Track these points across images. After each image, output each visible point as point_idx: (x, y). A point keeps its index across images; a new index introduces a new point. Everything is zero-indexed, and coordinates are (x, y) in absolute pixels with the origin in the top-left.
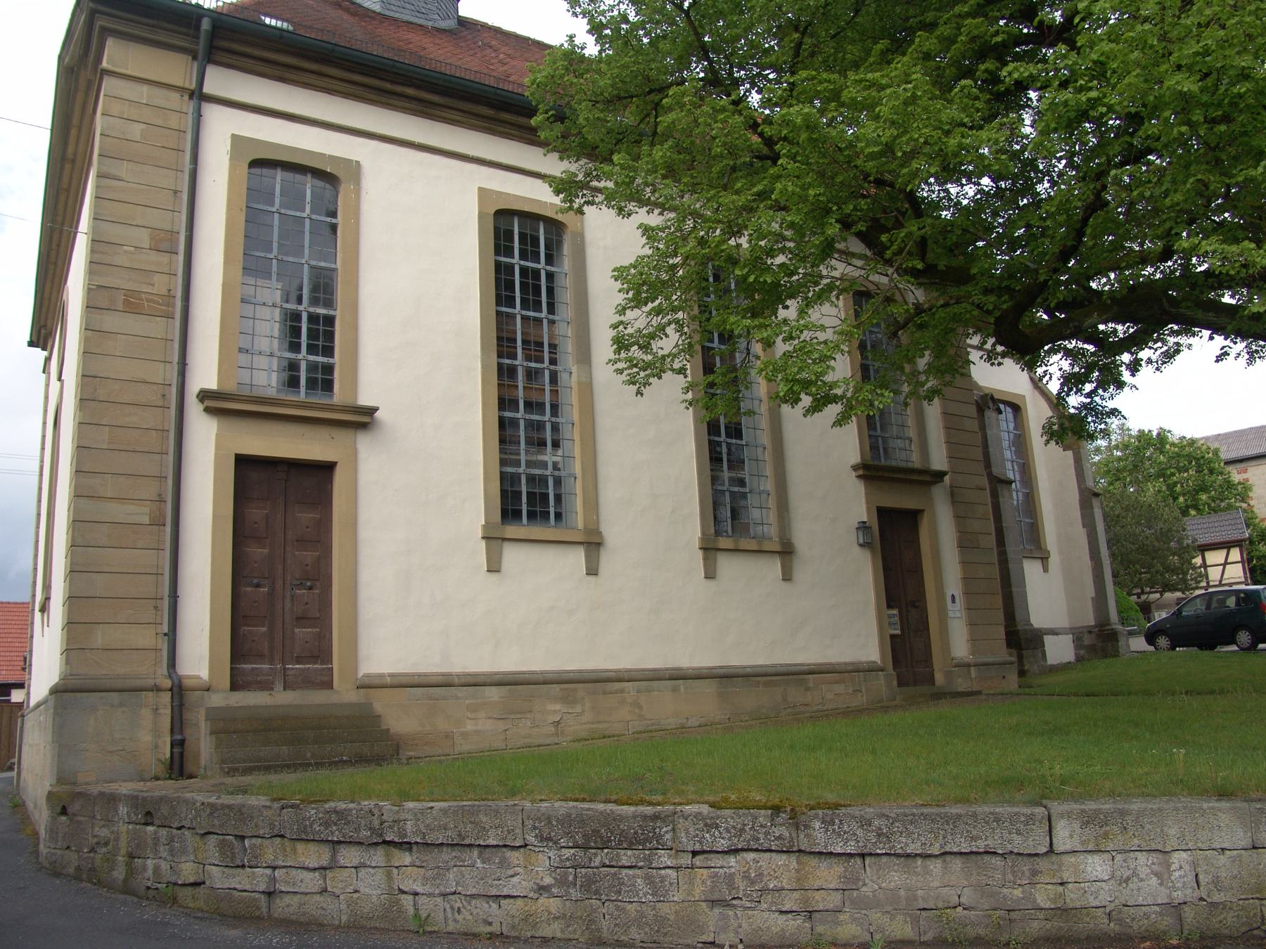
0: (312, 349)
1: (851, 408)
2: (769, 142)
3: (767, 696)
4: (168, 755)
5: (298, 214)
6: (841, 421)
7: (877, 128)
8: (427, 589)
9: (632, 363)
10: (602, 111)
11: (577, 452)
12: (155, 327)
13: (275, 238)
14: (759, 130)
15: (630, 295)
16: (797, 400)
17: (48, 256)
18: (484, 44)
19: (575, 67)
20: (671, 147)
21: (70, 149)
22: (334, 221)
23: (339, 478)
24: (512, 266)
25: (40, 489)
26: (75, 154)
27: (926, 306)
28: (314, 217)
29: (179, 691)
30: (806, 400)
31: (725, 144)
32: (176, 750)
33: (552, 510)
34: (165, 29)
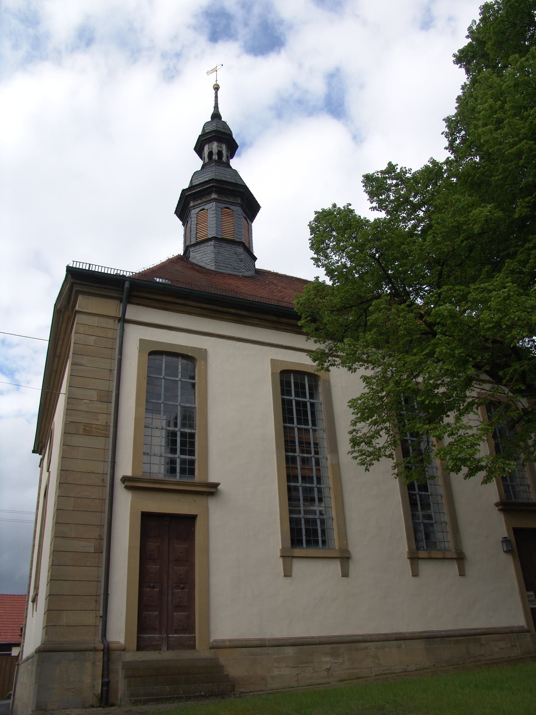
0: (183, 452)
1: (492, 473)
2: (430, 325)
3: (456, 650)
4: (100, 692)
5: (174, 379)
6: (485, 481)
7: (490, 314)
8: (251, 589)
9: (362, 453)
10: (336, 315)
11: (333, 504)
12: (98, 443)
13: (163, 392)
14: (424, 319)
15: (359, 414)
16: (459, 470)
17: (45, 404)
18: (270, 282)
19: (320, 293)
20: (375, 332)
21: (58, 351)
22: (193, 381)
23: (199, 524)
24: (291, 400)
25: (35, 531)
26: (61, 353)
27: (530, 410)
28: (183, 380)
29: (108, 651)
30: (465, 470)
31: (405, 329)
32: (104, 688)
33: (320, 539)
34: (107, 289)
